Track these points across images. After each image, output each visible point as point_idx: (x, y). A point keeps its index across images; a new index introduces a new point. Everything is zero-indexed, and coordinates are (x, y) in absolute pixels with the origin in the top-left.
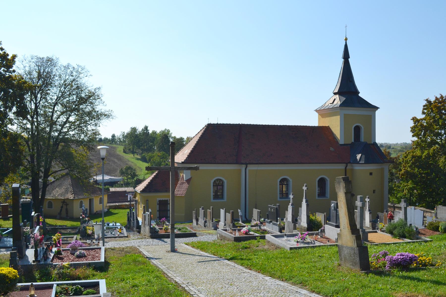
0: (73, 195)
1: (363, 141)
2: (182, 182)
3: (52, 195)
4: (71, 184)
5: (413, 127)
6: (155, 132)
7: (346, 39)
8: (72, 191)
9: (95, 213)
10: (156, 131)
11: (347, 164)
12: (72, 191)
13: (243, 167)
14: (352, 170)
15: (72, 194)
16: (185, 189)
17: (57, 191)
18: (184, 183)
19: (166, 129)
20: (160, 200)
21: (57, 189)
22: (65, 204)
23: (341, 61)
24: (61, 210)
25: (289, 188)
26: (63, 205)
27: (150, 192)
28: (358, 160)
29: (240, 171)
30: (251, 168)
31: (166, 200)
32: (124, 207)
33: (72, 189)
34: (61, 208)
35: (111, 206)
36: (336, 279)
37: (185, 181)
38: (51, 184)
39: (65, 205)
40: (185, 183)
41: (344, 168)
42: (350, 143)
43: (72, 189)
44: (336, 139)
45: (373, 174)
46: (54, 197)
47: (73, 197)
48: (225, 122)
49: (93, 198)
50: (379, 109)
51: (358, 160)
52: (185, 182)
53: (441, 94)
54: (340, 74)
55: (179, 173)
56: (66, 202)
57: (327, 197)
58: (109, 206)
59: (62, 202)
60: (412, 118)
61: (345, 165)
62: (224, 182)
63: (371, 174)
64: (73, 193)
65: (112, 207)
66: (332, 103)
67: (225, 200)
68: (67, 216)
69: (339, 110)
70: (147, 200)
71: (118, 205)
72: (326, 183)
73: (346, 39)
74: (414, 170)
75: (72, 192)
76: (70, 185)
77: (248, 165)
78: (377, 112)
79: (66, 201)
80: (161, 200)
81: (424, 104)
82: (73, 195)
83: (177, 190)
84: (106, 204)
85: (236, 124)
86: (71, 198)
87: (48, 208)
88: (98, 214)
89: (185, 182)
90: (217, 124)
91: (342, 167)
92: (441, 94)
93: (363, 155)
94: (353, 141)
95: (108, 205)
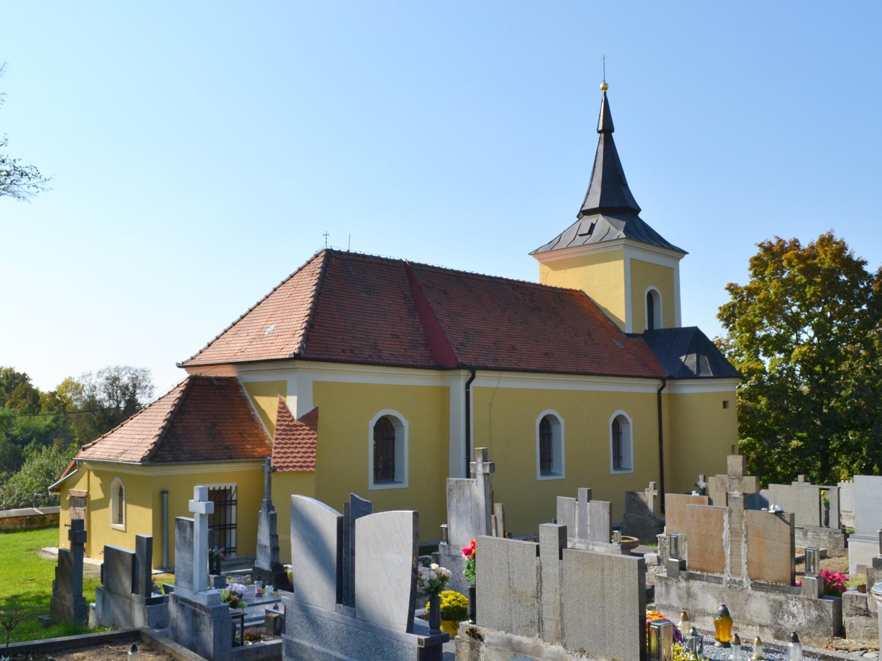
1: (662, 327)
2: (287, 425)
5: (729, 307)
7: (605, 88)
11: (664, 380)
13: (457, 381)
14: (672, 397)
16: (309, 448)
18: (295, 426)
20: (211, 489)
23: (593, 143)
27: (177, 460)
28: (695, 373)
29: (444, 393)
30: (484, 381)
31: (225, 490)
37: (299, 420)
40: (301, 426)
41: (654, 391)
42: (642, 332)
44: (612, 322)
45: (730, 404)
48: (368, 252)
50: (687, 255)
51: (695, 373)
52: (299, 423)
53: (776, 237)
54: (594, 166)
55: (247, 394)
57: (630, 469)
60: (726, 286)
61: (657, 383)
62: (401, 425)
63: (725, 404)
66: (587, 232)
67: (405, 484)
69: (621, 247)
70: (164, 492)
72: (397, 435)
73: (606, 86)
74: (759, 402)
77: (478, 374)
78: (683, 263)
80: (214, 490)
81: (755, 254)
83: (279, 453)
85: (394, 261)
89: (299, 423)
90: (348, 253)
91: (649, 388)
92: (776, 237)
93: (701, 356)
94: (647, 329)
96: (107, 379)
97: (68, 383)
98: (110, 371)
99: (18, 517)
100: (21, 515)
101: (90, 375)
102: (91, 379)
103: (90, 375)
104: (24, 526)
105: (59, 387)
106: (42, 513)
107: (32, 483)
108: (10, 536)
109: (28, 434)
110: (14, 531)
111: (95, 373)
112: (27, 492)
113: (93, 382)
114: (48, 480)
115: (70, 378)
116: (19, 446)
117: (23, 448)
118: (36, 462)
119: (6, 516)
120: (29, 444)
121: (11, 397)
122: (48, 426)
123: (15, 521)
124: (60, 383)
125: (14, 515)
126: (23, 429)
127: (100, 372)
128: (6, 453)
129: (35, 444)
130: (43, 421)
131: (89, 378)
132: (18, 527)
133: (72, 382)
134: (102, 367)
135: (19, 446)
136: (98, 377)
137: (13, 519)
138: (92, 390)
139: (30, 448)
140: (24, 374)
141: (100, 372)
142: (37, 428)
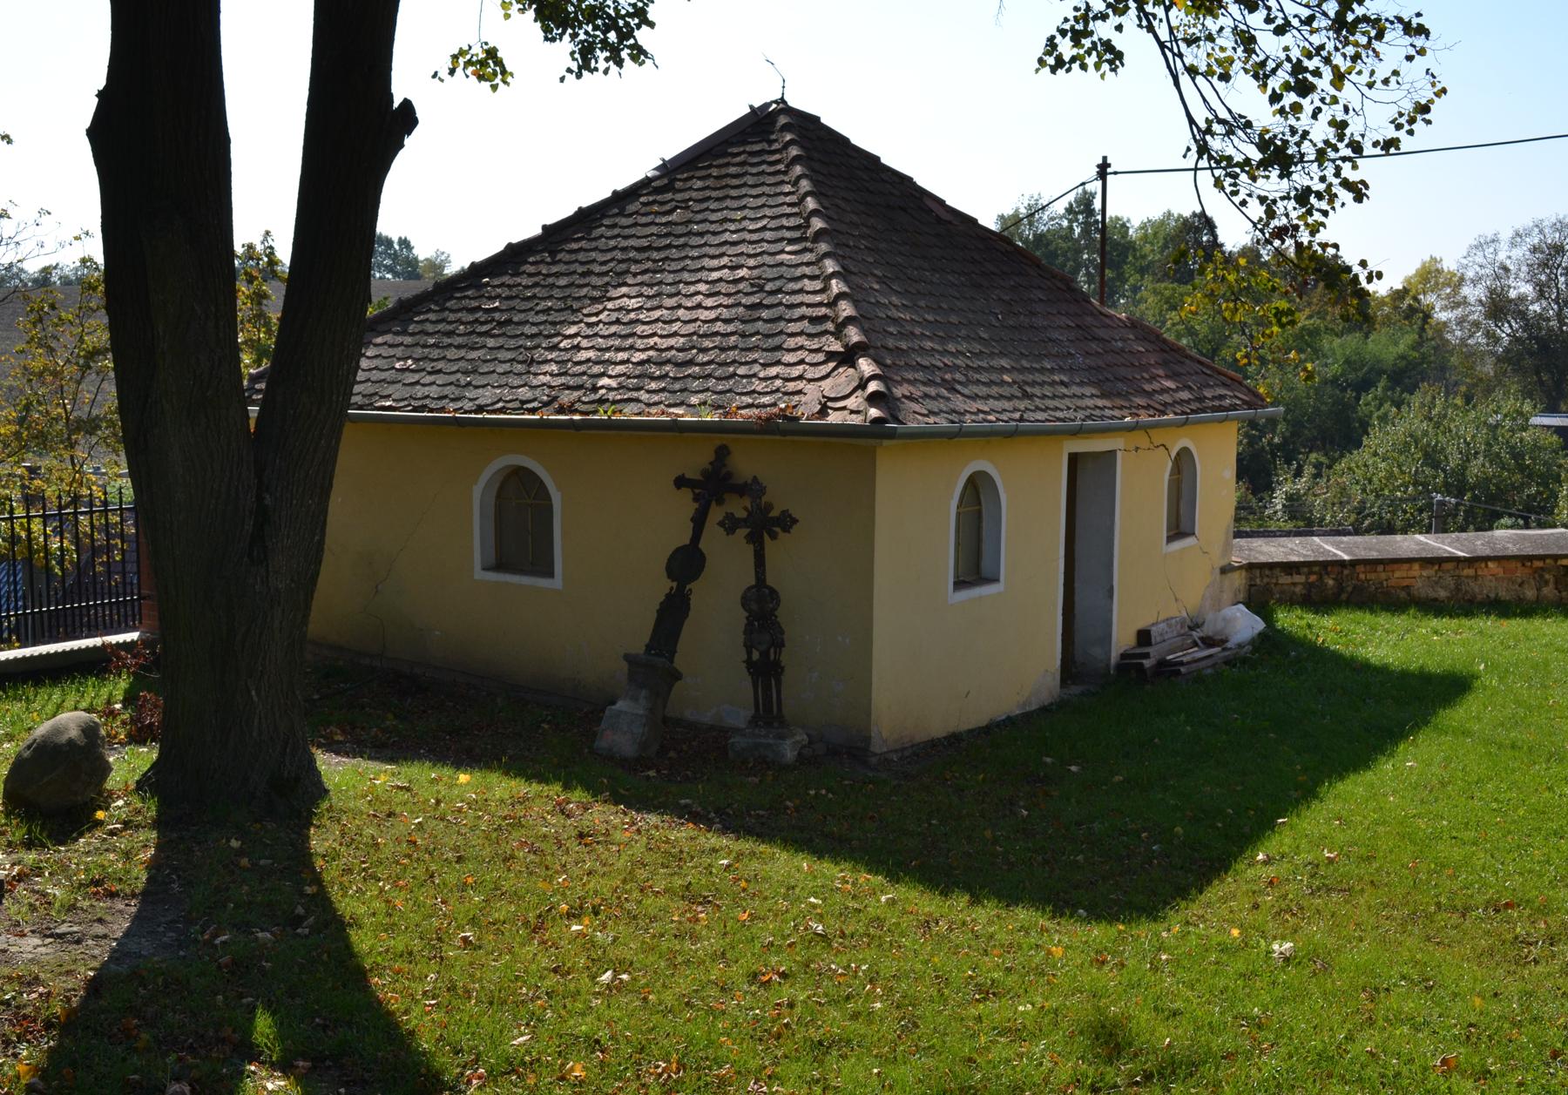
0: (866, 366)
3: (546, 375)
4: (817, 224)
6: (1124, 225)
8: (846, 309)
9: (1130, 665)
10: (1129, 221)
12: (846, 309)
15: (847, 358)
17: (627, 329)
19: (1169, 214)
21: (627, 298)
22: (738, 507)
24: (673, 612)
25: (986, 547)
26: (699, 521)
32: (1419, 580)
33: (836, 286)
34: (665, 585)
35: (1272, 566)
36: (51, 350)
38: (553, 253)
39: (730, 525)
43: (836, 286)
46: (567, 397)
47: (874, 399)
49: (1112, 454)
56: (752, 489)
58: (1251, 567)
59: (681, 482)
64: (854, 335)
65: (1285, 580)
68: (768, 714)
71: (1354, 563)
75: (838, 333)
76: (802, 238)
79: (744, 465)
82: (866, 366)
84: (1227, 549)
86: (834, 418)
87: (499, 566)
88: (1166, 669)
95: (1236, 559)
96: (1534, 250)
97: (1429, 273)
98: (1541, 232)
99: (1531, 558)
100: (1541, 552)
101: (1493, 241)
102: (1496, 252)
103: (1493, 241)
104: (1549, 591)
105: (1408, 280)
106: (1346, 557)
107: (1391, 476)
108: (1515, 625)
109: (1360, 374)
110: (1526, 609)
111: (1506, 235)
112: (1377, 496)
113: (1502, 256)
114: (1428, 471)
115: (1433, 259)
116: (1350, 394)
117: (1358, 399)
118: (1399, 430)
119: (1487, 552)
120: (1373, 389)
121: (1309, 304)
122: (1403, 357)
123: (1521, 573)
124: (1411, 271)
125: (1513, 549)
126: (1347, 361)
127: (1518, 234)
128: (1323, 408)
129: (1386, 389)
130: (1387, 346)
131: (1491, 250)
132: (1530, 593)
133: (1437, 270)
134: (1523, 222)
135: (1350, 394)
136: (1513, 245)
137: (1513, 565)
138: (1498, 277)
139: (1375, 398)
140: (789, 532)
141: (1518, 234)
142: (1378, 362)
